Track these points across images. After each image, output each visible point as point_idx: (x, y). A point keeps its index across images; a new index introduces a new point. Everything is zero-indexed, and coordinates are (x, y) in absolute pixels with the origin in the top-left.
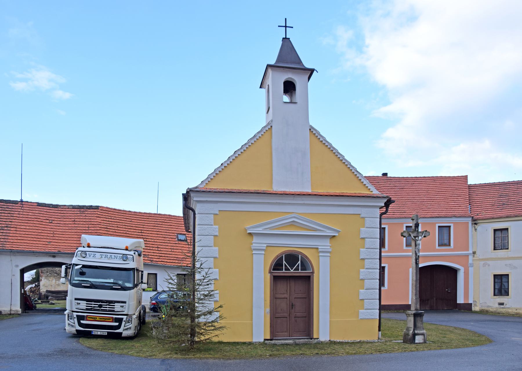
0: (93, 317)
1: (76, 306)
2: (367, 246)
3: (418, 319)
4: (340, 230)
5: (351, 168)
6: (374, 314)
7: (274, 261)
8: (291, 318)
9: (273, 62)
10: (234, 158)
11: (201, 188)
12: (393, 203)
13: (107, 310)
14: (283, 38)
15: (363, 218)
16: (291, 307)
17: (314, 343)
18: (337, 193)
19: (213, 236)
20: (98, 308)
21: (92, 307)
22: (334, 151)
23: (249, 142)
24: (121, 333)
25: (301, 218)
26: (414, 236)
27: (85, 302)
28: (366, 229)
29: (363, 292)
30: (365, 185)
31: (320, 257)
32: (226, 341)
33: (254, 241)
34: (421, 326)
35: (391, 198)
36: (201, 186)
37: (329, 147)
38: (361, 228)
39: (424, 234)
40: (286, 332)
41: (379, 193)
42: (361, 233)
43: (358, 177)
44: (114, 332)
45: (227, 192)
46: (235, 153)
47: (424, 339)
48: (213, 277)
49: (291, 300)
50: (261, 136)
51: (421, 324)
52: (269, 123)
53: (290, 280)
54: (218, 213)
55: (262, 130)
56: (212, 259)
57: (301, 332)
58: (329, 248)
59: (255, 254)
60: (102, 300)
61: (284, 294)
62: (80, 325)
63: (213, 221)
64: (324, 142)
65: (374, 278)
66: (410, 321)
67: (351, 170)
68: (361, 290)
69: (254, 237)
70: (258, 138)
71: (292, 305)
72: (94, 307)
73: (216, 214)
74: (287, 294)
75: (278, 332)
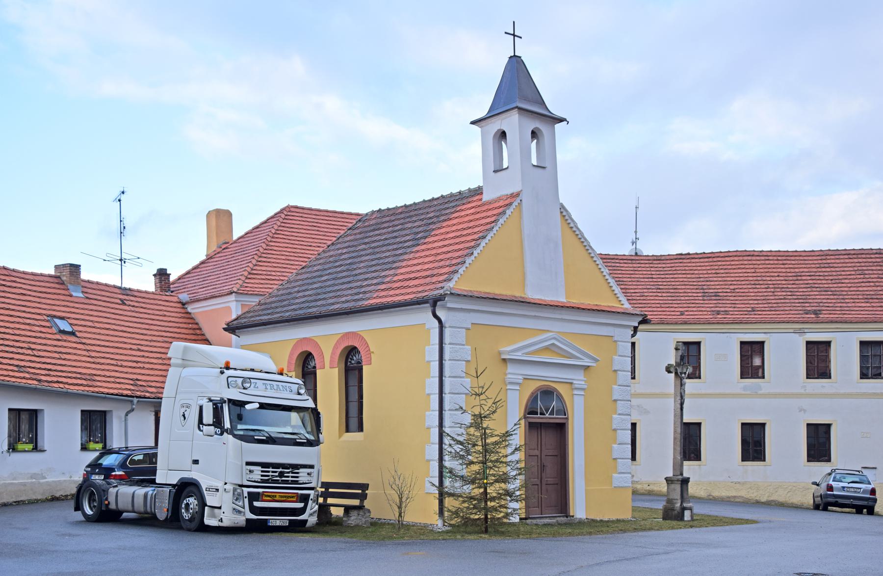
0: (271, 494)
1: (248, 476)
4: (598, 358)
13: (288, 481)
15: (616, 341)
20: (278, 478)
21: (268, 476)
22: (585, 244)
24: (306, 521)
25: (562, 340)
27: (260, 468)
28: (619, 357)
31: (509, 392)
37: (580, 236)
38: (614, 357)
44: (297, 520)
54: (470, 326)
58: (583, 383)
59: (576, 394)
60: (284, 464)
62: (253, 510)
64: (574, 229)
65: (626, 427)
66: (674, 490)
68: (614, 445)
69: (508, 364)
71: (544, 466)
72: (272, 476)
73: (468, 329)
74: (538, 450)
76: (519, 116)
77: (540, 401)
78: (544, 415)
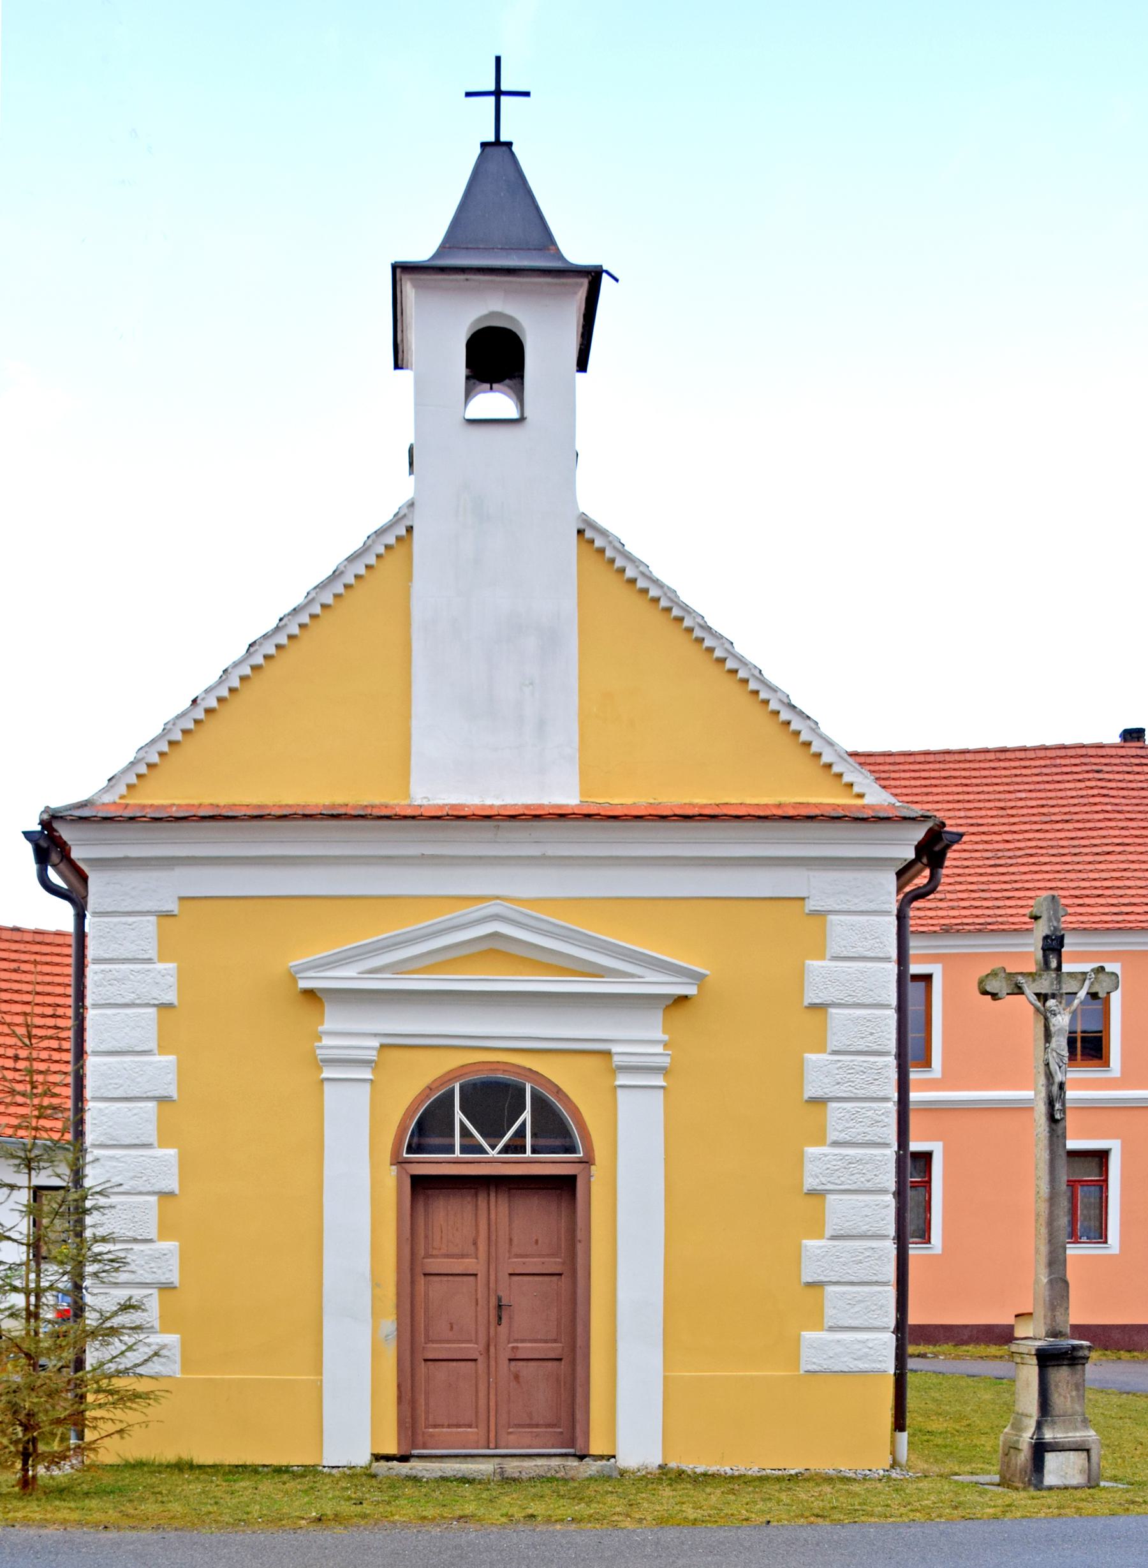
2: (833, 1044)
3: (1061, 1375)
5: (763, 695)
6: (872, 1352)
7: (415, 1112)
8: (493, 1363)
9: (423, 250)
10: (247, 671)
11: (103, 804)
12: (957, 842)
14: (484, 145)
16: (493, 1313)
17: (587, 1475)
18: (693, 806)
19: (154, 1005)
22: (687, 623)
23: (313, 600)
26: (1037, 994)
29: (818, 1251)
30: (829, 766)
31: (619, 1091)
32: (210, 1461)
33: (327, 1026)
35: (943, 825)
36: (107, 799)
37: (664, 603)
39: (1087, 983)
40: (470, 1426)
41: (893, 800)
42: (806, 984)
43: (797, 733)
45: (204, 818)
46: (252, 649)
47: (1089, 1469)
48: (153, 1181)
49: (492, 1285)
50: (362, 571)
51: (1072, 1401)
52: (398, 513)
53: (489, 1195)
54: (173, 906)
55: (370, 546)
56: (152, 1105)
57: (537, 1426)
58: (659, 1049)
59: (621, 1086)
61: (463, 1256)
63: (155, 943)
64: (641, 583)
67: (766, 702)
68: (808, 1243)
70: (350, 579)
73: (168, 915)
75: (435, 1426)
76: (416, 293)
77: (462, 1109)
78: (484, 1152)
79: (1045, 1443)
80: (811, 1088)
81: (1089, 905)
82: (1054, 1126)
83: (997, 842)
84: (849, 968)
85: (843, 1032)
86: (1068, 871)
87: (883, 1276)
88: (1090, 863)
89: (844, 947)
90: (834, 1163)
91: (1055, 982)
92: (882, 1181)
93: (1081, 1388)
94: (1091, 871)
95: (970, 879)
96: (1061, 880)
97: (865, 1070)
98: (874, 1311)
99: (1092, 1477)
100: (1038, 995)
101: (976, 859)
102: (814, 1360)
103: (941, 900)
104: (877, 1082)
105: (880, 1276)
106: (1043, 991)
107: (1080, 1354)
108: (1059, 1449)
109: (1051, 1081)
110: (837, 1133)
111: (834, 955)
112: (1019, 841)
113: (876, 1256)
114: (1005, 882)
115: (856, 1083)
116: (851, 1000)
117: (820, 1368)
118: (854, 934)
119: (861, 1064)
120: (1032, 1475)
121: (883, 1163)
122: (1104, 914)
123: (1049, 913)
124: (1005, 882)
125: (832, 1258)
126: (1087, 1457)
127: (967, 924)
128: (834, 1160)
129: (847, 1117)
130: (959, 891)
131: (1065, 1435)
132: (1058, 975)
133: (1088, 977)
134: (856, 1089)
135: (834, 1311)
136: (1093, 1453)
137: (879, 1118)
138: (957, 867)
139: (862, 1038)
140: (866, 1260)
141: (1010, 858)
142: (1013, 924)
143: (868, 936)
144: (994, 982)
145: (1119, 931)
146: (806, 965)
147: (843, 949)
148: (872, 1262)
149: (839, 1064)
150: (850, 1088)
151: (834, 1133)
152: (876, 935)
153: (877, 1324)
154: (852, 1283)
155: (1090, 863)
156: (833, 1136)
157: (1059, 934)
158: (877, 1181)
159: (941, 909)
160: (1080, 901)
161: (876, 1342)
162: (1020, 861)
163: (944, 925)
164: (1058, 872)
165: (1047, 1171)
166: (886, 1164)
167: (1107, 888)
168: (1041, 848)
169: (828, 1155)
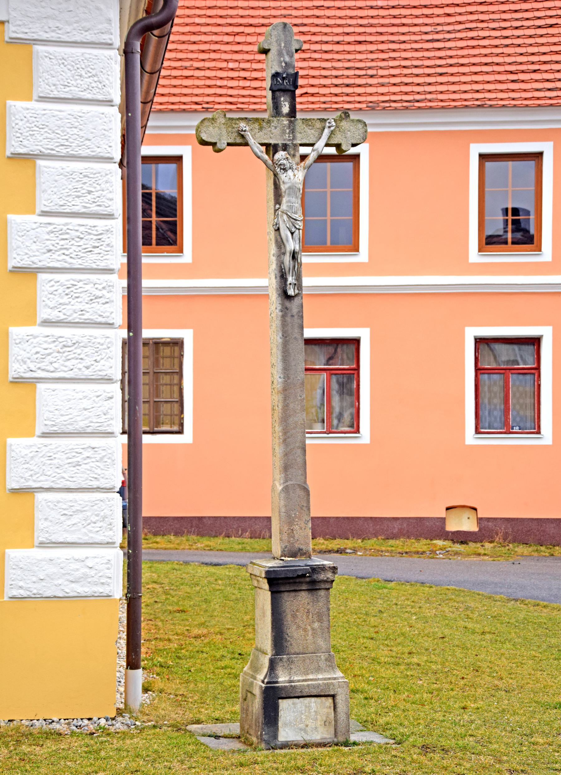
2: (42, 204)
6: (93, 573)
29: (27, 451)
34: (321, 642)
39: (326, 132)
42: (8, 128)
65: (87, 373)
79: (278, 687)
80: (15, 256)
81: (523, 81)
82: (287, 304)
83: (438, 16)
84: (60, 111)
85: (55, 190)
86: (507, 46)
87: (107, 481)
88: (530, 37)
89: (54, 85)
90: (45, 346)
91: (288, 131)
92: (104, 368)
93: (325, 618)
94: (531, 45)
95: (404, 55)
96: (497, 55)
97: (82, 236)
98: (95, 523)
99: (339, 729)
100: (267, 146)
101: (414, 33)
102: (21, 584)
103: (372, 76)
104: (97, 251)
105: (102, 480)
106: (272, 142)
107: (322, 576)
108: (297, 695)
109: (283, 251)
110: (50, 310)
111: (41, 95)
112: (460, 14)
113: (98, 457)
114: (440, 58)
115: (71, 251)
116: (65, 151)
117: (29, 593)
118: (65, 69)
119: (77, 228)
120: (263, 729)
121: (105, 346)
122: (537, 90)
123: (280, 45)
124: (440, 58)
125: (42, 459)
126: (332, 705)
127: (395, 101)
128: (45, 342)
129: (60, 291)
130: (392, 67)
131: (304, 678)
132: (291, 122)
133: (328, 124)
134: (71, 257)
135: (47, 524)
136: (339, 699)
137: (99, 294)
138: (393, 42)
139: (78, 197)
140: (85, 462)
141: (449, 32)
142: (442, 101)
143: (83, 73)
144: (211, 129)
145: (551, 108)
146: (8, 105)
147: (53, 88)
148: (92, 464)
149: (51, 228)
150: (64, 257)
151: (45, 310)
152: (94, 72)
153: (99, 538)
154: (69, 490)
155: (530, 37)
156: (43, 313)
157: (291, 71)
158: (97, 368)
159: (371, 85)
160: (514, 77)
161: (97, 560)
162: (459, 35)
163: (371, 102)
164: (496, 46)
165: (280, 357)
166: (109, 348)
167: (545, 63)
168: (482, 21)
169: (38, 337)
